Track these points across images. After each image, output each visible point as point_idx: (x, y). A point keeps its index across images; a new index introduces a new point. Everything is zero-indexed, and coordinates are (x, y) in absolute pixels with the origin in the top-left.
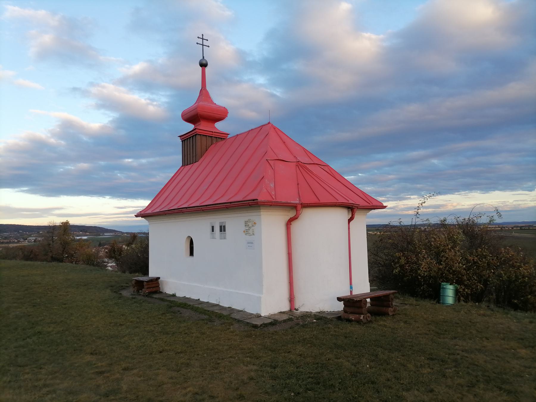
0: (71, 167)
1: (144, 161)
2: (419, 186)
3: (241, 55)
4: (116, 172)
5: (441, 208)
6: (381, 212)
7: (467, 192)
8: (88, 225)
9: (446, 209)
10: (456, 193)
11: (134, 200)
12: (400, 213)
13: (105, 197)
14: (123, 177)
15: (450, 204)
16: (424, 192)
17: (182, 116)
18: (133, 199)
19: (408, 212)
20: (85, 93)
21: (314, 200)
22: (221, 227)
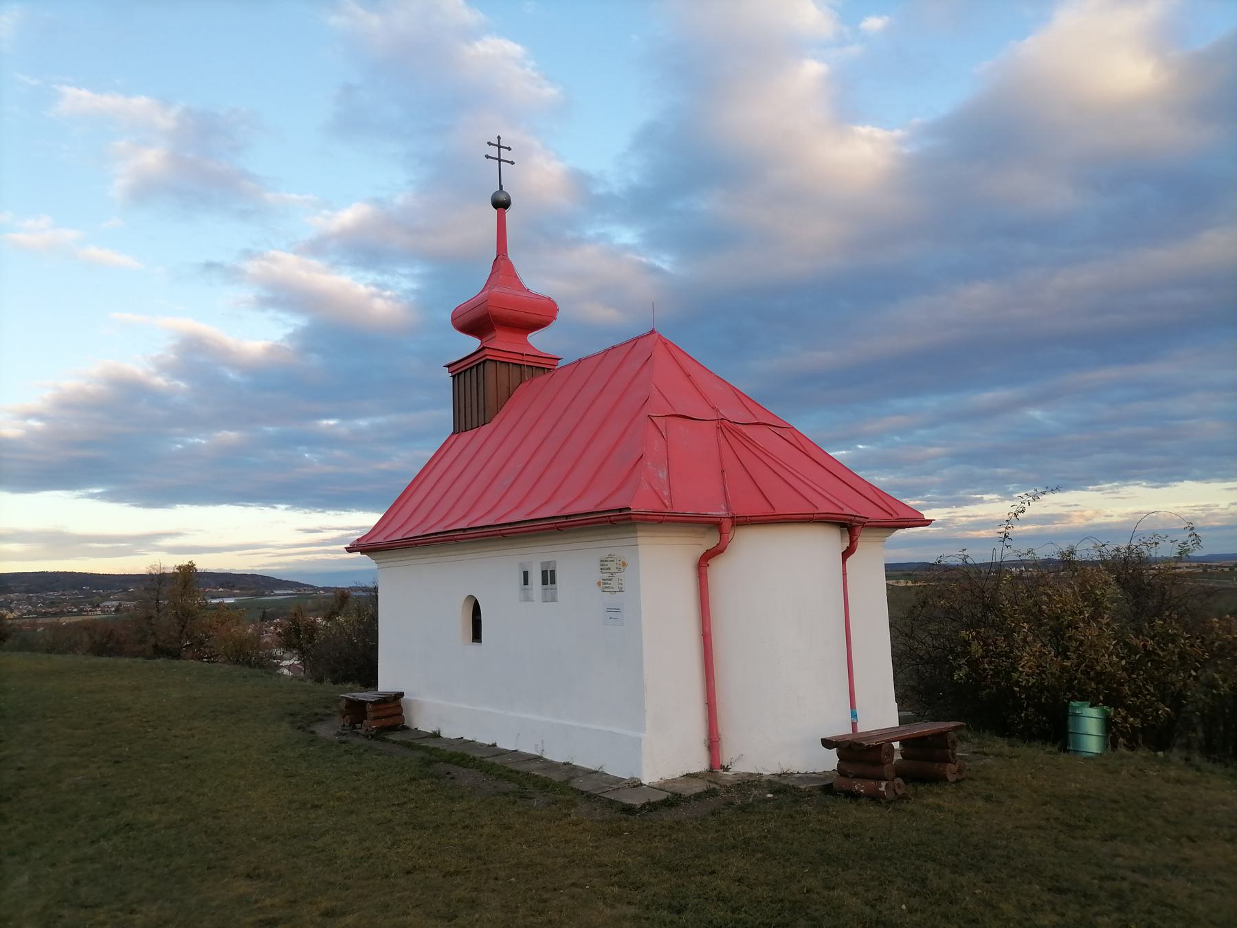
0: (199, 440)
1: (363, 423)
3: (579, 182)
4: (301, 448)
7: (1116, 484)
9: (1067, 525)
10: (1090, 487)
11: (342, 512)
12: (959, 535)
13: (275, 508)
15: (1076, 513)
17: (452, 320)
20: (232, 274)
21: (805, 509)
22: (544, 573)
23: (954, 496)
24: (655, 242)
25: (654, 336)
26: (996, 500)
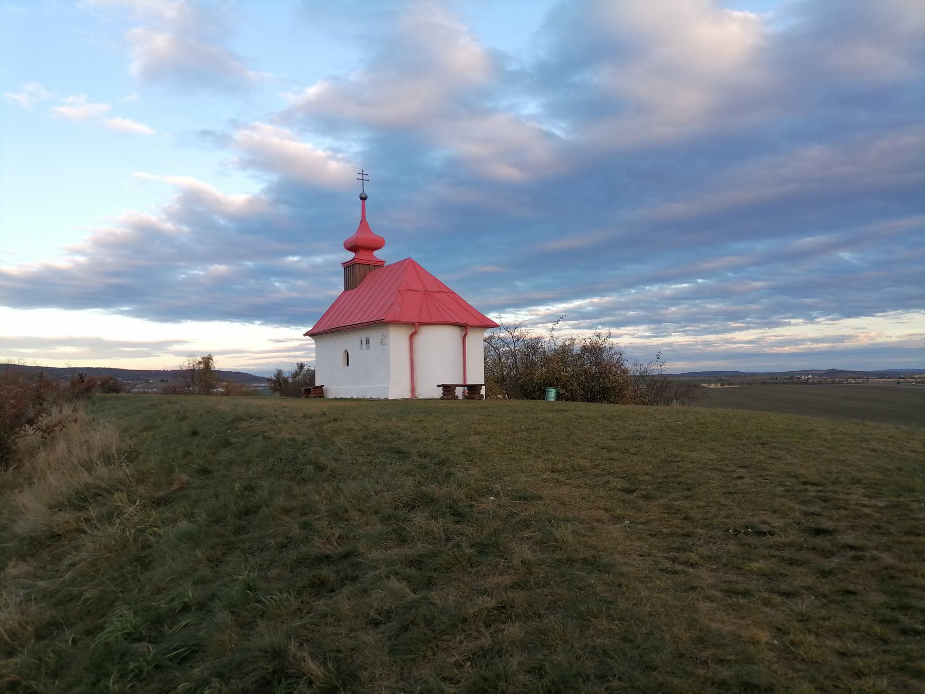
0: (198, 272)
1: (319, 260)
2: (808, 301)
3: (496, 60)
4: (273, 279)
5: (846, 341)
6: (732, 348)
7: (899, 311)
8: (225, 369)
9: (854, 343)
10: (878, 314)
11: (301, 327)
12: (768, 350)
13: (253, 323)
14: (283, 288)
15: (863, 335)
16: (818, 312)
17: (344, 245)
18: (300, 326)
19: (783, 349)
20: (223, 141)
21: (442, 320)
23: (768, 320)
24: (555, 111)
25: (409, 260)
26: (802, 324)
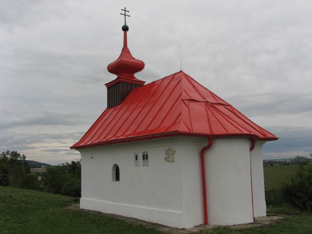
22: (144, 156)
